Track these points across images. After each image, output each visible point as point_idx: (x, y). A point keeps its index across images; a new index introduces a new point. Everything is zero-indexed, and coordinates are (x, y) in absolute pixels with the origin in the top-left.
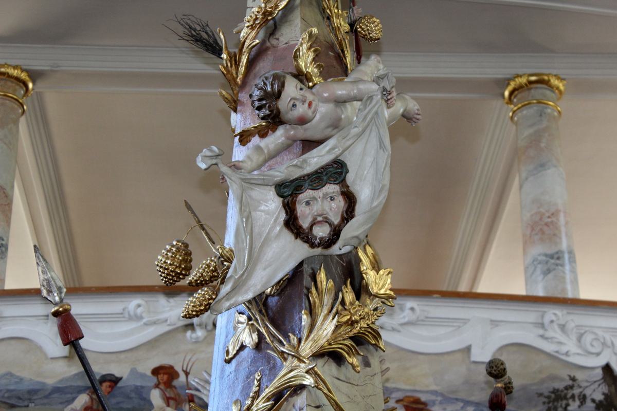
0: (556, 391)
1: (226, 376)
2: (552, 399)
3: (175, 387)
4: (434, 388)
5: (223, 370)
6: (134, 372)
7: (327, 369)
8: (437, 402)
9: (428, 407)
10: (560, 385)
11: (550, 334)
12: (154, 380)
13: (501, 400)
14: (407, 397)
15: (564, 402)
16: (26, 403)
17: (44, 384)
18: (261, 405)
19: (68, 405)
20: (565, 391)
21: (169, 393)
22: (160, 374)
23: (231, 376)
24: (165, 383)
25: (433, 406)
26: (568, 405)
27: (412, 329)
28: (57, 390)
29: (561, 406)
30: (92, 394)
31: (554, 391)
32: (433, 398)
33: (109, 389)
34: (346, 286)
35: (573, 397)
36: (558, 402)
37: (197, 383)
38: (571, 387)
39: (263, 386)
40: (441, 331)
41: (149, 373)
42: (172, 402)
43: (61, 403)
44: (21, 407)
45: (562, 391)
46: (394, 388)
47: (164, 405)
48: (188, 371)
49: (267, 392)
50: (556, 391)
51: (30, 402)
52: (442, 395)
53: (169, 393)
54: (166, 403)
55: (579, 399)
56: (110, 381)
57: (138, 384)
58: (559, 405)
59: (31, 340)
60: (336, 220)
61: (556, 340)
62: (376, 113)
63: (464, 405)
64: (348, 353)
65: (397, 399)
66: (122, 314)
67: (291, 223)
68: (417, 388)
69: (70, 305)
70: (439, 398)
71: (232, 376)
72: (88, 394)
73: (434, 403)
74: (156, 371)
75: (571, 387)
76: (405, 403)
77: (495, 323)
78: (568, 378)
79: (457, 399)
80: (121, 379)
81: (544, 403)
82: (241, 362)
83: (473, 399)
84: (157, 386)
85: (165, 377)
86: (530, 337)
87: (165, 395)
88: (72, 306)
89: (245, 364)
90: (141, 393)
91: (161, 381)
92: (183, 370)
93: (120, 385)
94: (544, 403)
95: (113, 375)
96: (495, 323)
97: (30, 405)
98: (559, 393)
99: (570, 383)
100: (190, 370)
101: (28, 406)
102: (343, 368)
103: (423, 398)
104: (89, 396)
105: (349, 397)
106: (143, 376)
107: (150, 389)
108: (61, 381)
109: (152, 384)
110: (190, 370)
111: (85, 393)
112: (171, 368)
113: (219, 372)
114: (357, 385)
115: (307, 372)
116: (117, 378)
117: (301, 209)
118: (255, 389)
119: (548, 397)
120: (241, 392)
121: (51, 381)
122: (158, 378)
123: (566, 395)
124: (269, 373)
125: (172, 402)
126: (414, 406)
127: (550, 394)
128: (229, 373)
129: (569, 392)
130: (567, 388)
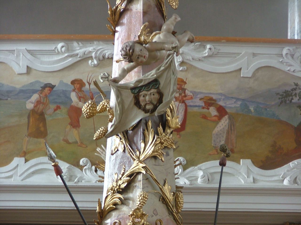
0: (286, 92)
1: (111, 161)
2: (284, 97)
3: (83, 91)
4: (220, 91)
5: (110, 158)
6: (61, 82)
7: (151, 164)
8: (222, 99)
9: (217, 102)
10: (289, 89)
11: (286, 59)
12: (72, 87)
13: (224, 163)
14: (205, 97)
15: (290, 98)
16: (6, 98)
17: (15, 87)
18: (125, 178)
19: (28, 99)
20: (292, 92)
21: (81, 94)
22: (76, 84)
23: (113, 161)
24: (78, 89)
25: (220, 101)
26: (292, 99)
27: (211, 60)
28: (21, 91)
29: (289, 100)
30: (40, 94)
31: (286, 92)
32: (220, 97)
33: (49, 92)
34: (160, 127)
35: (295, 95)
36: (287, 97)
37: (99, 150)
38: (295, 89)
39: (127, 169)
40: (226, 60)
41: (69, 83)
42: (82, 99)
43: (24, 98)
44: (4, 100)
45: (290, 92)
46: (199, 92)
47: (78, 101)
48: (90, 82)
49: (127, 173)
50: (286, 92)
51: (8, 97)
52: (224, 95)
53: (81, 94)
54: (79, 100)
55: (299, 96)
56: (49, 87)
57: (64, 89)
58: (288, 99)
59: (6, 63)
60: (155, 103)
61: (289, 64)
62: (172, 61)
63: (236, 100)
64: (159, 156)
65: (200, 98)
66: (54, 50)
67: (137, 103)
68: (211, 92)
69: (58, 162)
70: (223, 97)
71: (114, 161)
72: (38, 94)
73: (220, 99)
74: (73, 82)
75: (295, 89)
76: (205, 100)
77: (254, 55)
78: (294, 84)
79: (232, 98)
80: (55, 86)
81: (279, 98)
82: (117, 156)
83: (241, 97)
84: (74, 90)
85: (78, 86)
86: (274, 63)
87: (79, 95)
88: (59, 163)
89: (119, 157)
90: (66, 95)
91: (76, 88)
92: (87, 82)
93: (54, 89)
94: (279, 98)
95: (51, 84)
96: (254, 55)
97: (8, 99)
98: (288, 93)
99: (295, 87)
100: (91, 83)
101: (7, 99)
102: (157, 161)
103: (214, 97)
104: (38, 95)
105: (160, 171)
106: (66, 85)
107: (70, 92)
108: (23, 87)
109: (71, 89)
110: (91, 83)
111: (36, 93)
112: (81, 80)
113: (109, 158)
114: (163, 165)
115: (143, 167)
116: (53, 85)
117: (141, 98)
118: (123, 171)
119: (282, 95)
120: (118, 169)
121: (18, 87)
122: (74, 86)
123: (292, 93)
124: (128, 163)
125: (82, 99)
126: (210, 102)
127: (283, 94)
128: (113, 160)
129: (293, 92)
130: (293, 90)
